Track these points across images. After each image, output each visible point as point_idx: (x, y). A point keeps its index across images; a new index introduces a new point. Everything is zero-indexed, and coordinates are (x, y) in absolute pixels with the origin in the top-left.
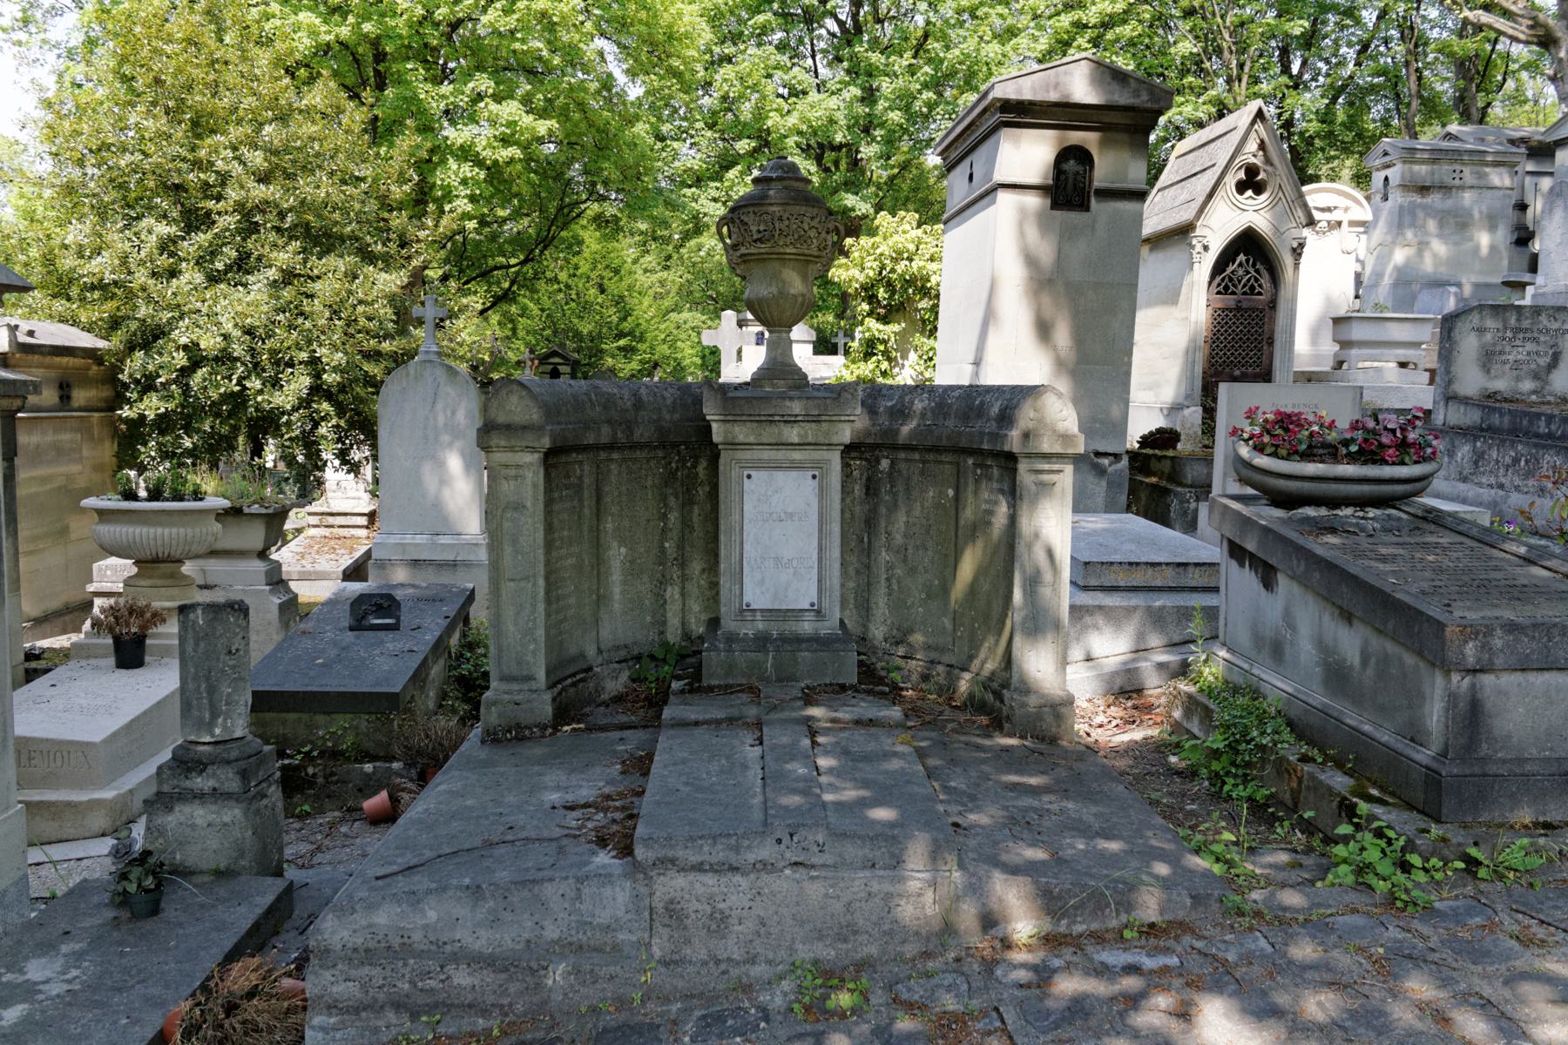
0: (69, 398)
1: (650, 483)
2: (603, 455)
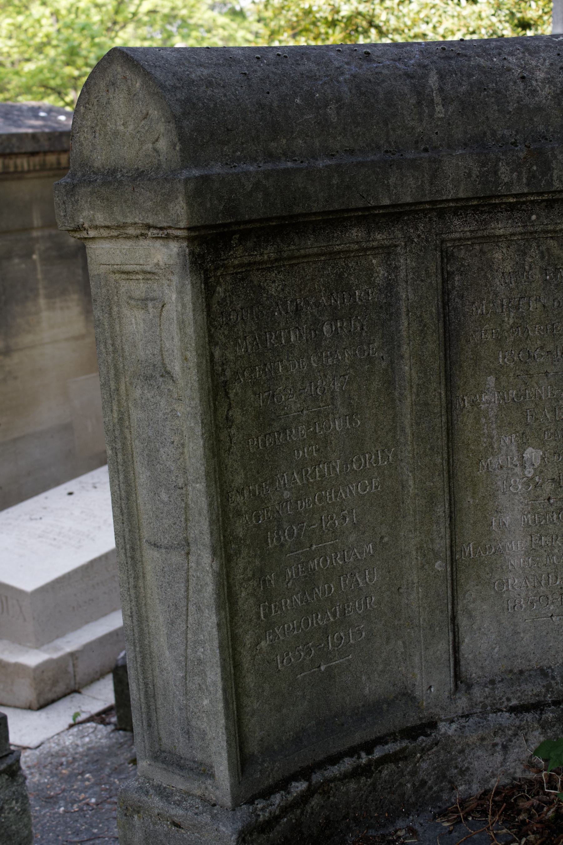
2: (460, 228)
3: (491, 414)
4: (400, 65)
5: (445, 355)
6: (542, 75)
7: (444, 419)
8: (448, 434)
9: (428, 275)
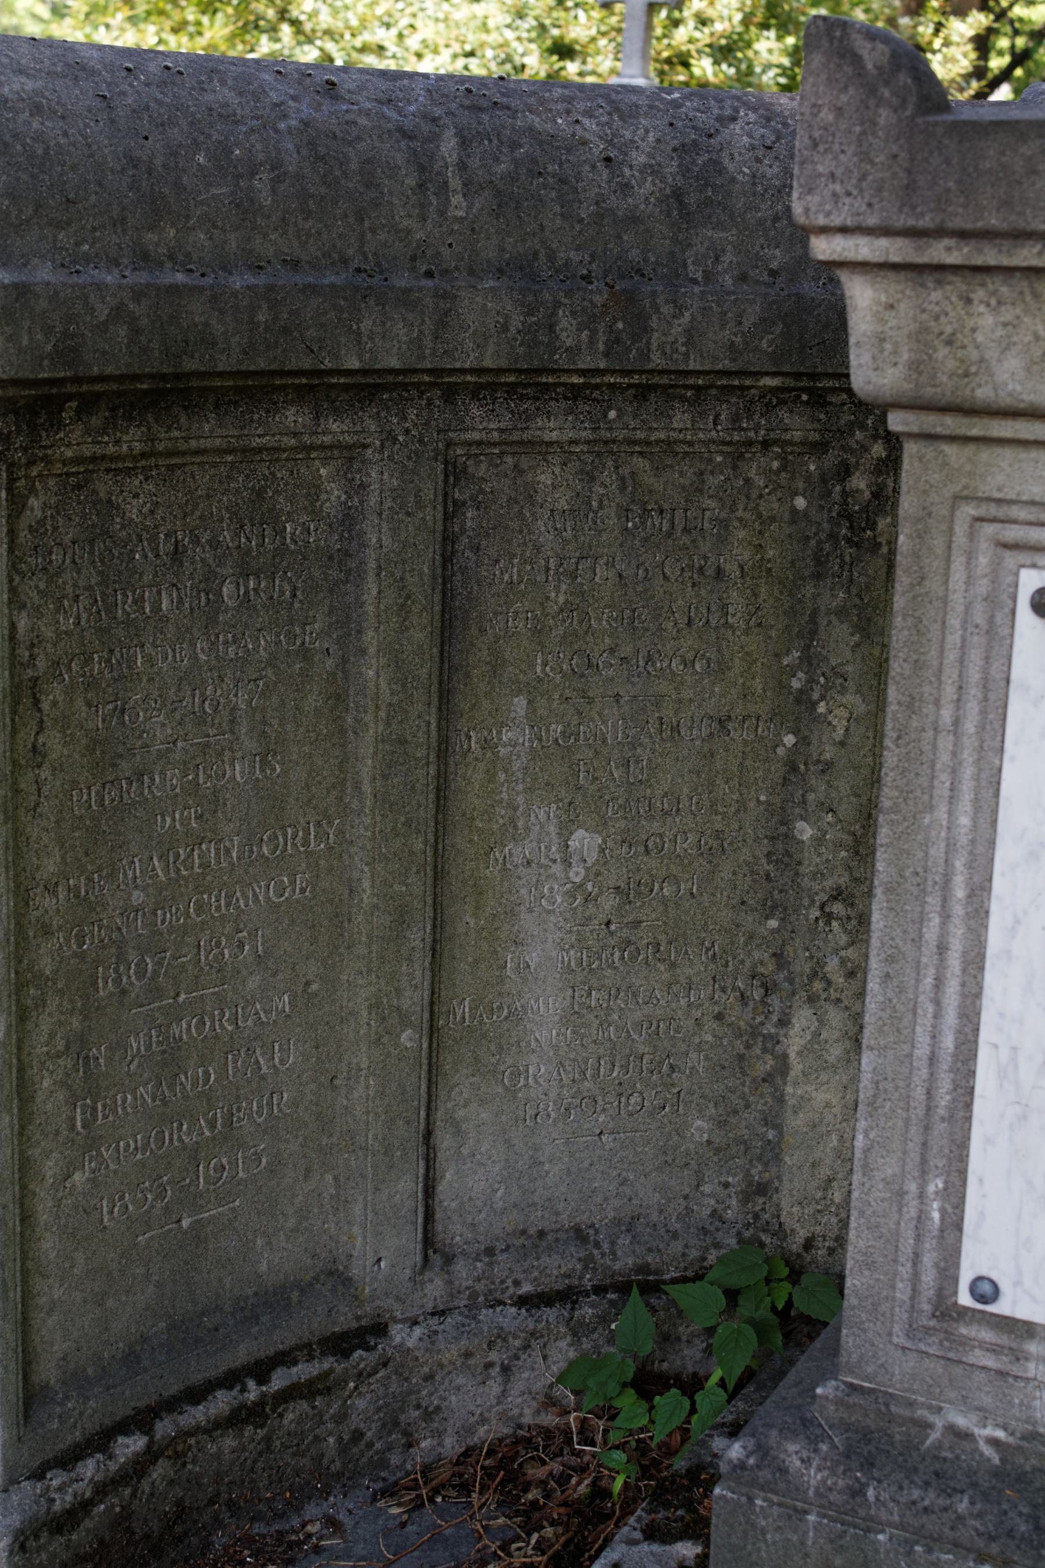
1: (738, 553)
2: (482, 422)
3: (517, 765)
6: (642, 159)
7: (432, 771)
9: (419, 504)
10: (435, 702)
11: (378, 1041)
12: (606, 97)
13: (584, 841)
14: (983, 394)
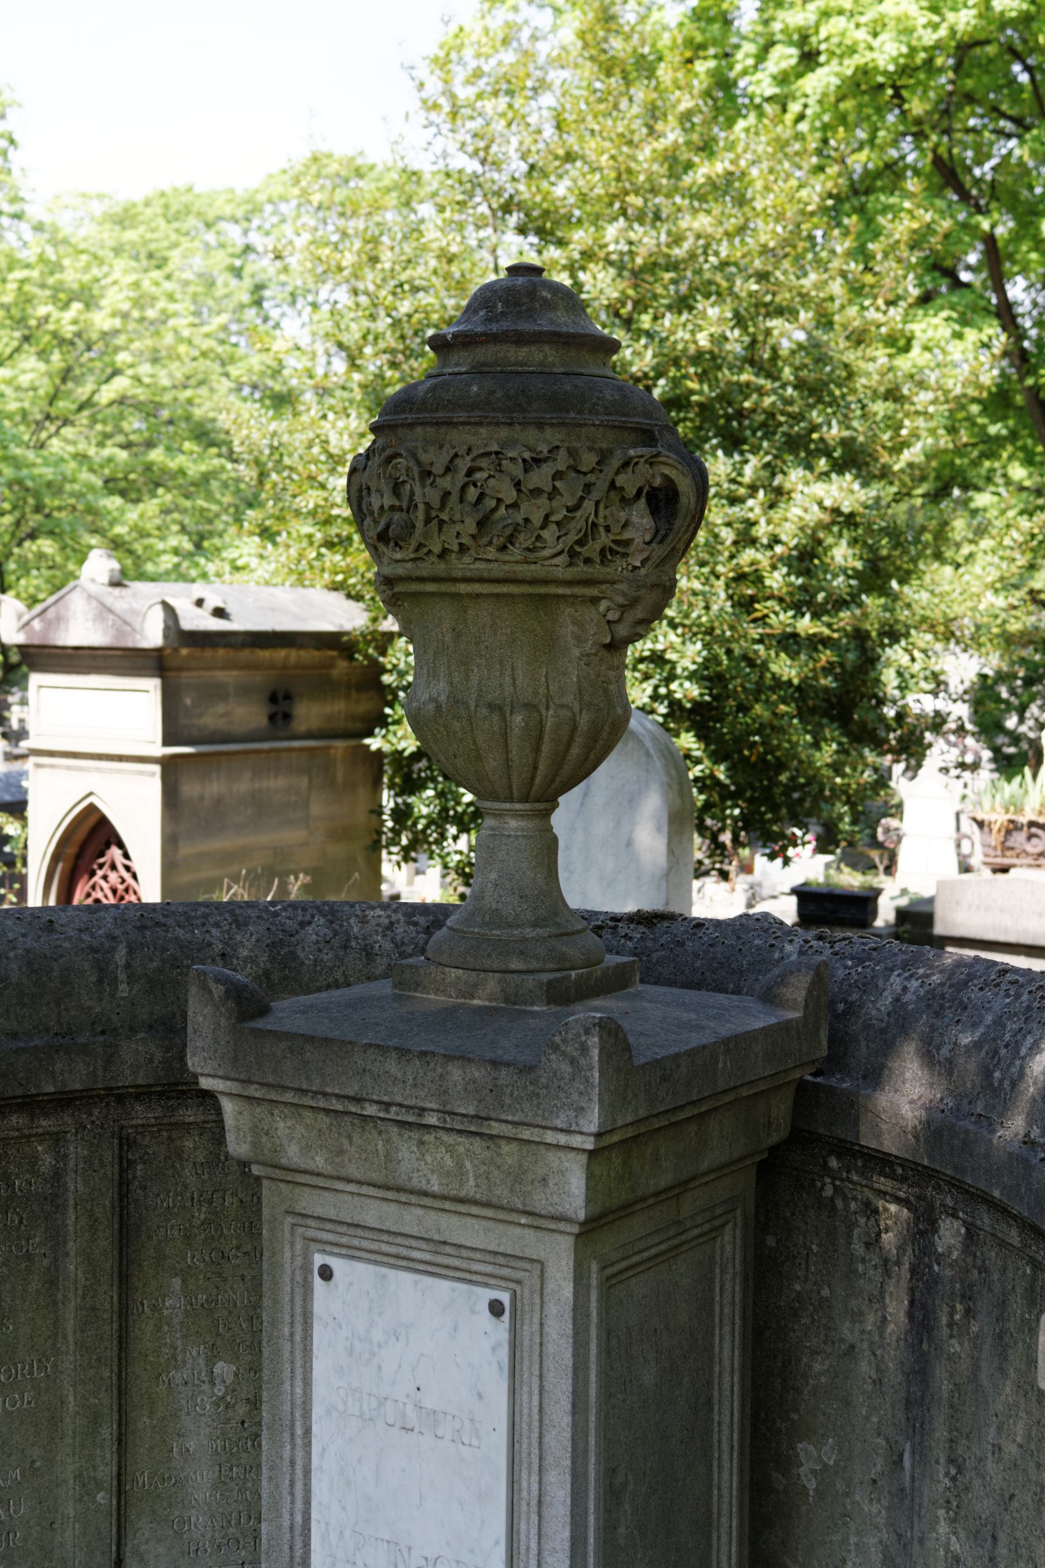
0: (287, 717)
2: (142, 1114)
3: (176, 1321)
4: (86, 937)
5: (120, 1254)
6: (246, 953)
7: (115, 1326)
8: (120, 1342)
9: (102, 1165)
10: (116, 1283)
11: (81, 1500)
12: (232, 912)
13: (223, 1368)
14: (284, 1161)
